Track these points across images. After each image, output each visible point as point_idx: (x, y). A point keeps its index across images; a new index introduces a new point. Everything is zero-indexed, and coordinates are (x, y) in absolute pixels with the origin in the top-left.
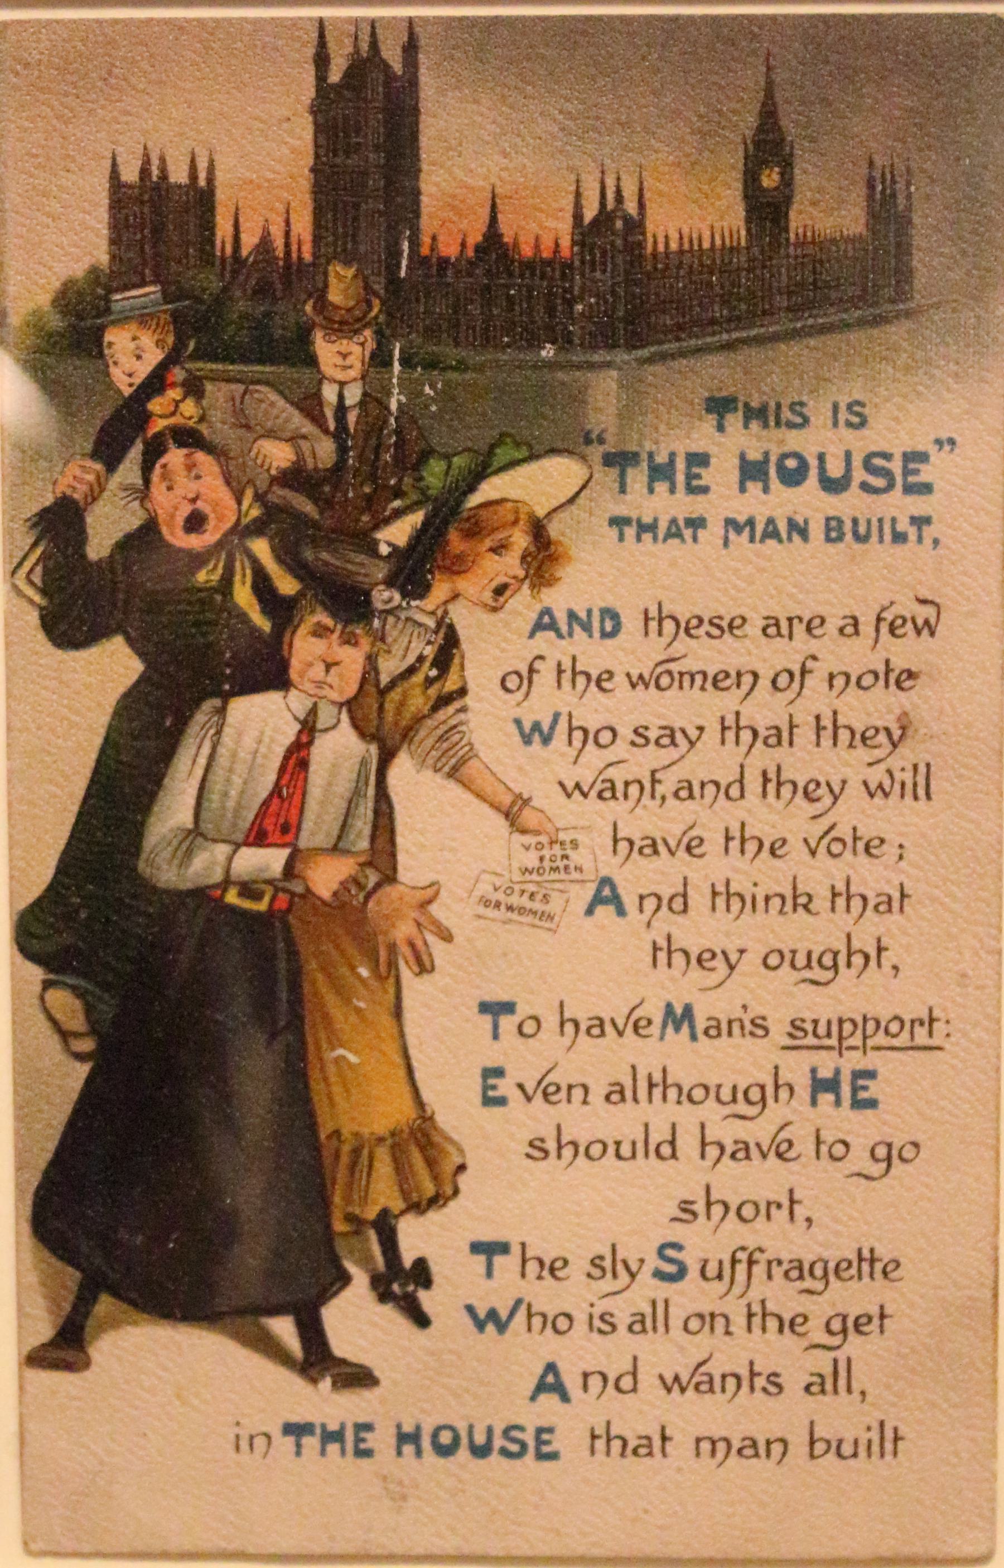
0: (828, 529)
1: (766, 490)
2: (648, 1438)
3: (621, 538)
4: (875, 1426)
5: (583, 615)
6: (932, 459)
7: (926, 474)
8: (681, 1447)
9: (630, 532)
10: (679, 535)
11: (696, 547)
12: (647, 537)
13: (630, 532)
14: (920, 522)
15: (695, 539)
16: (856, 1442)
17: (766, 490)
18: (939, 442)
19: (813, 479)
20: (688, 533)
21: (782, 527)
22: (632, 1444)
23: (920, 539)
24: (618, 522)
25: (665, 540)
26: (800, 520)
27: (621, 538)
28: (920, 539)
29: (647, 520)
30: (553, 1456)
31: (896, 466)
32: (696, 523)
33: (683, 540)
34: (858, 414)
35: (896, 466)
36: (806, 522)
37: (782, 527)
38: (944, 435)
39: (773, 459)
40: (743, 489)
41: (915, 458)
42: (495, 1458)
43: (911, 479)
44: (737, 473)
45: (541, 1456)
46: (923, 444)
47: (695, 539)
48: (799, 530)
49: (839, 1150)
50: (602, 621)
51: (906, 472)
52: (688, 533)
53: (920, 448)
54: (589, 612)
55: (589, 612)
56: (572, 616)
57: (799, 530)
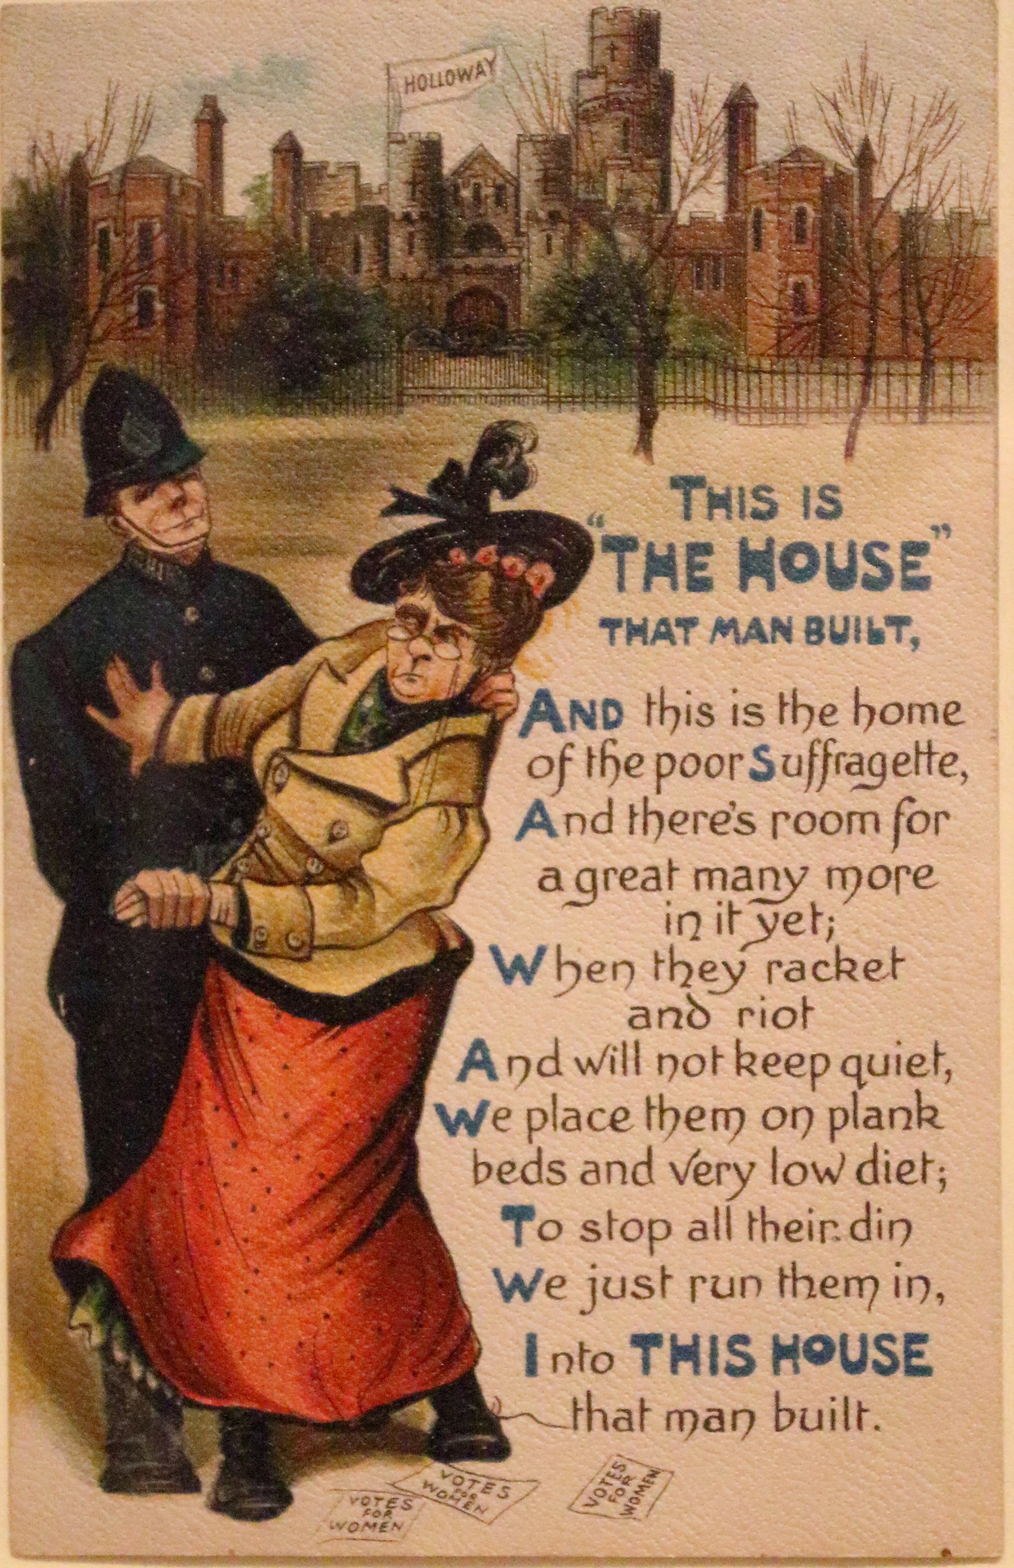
0: (808, 633)
1: (771, 586)
2: (628, 1412)
3: (612, 638)
4: (840, 1400)
5: (586, 706)
6: (933, 547)
7: (927, 564)
8: (655, 1418)
9: (621, 633)
10: (668, 636)
11: (688, 648)
12: (637, 641)
13: (621, 633)
14: (899, 622)
15: (686, 641)
16: (820, 1413)
17: (771, 586)
18: (935, 528)
19: (822, 575)
20: (678, 632)
21: (767, 628)
22: (612, 1416)
23: (899, 639)
24: (610, 624)
25: (654, 640)
26: (784, 620)
27: (612, 638)
28: (899, 639)
29: (637, 621)
30: (926, 1371)
31: (893, 559)
32: (688, 623)
33: (673, 643)
34: (832, 501)
35: (893, 559)
36: (790, 619)
37: (767, 628)
38: (939, 523)
39: (778, 550)
40: (744, 586)
41: (915, 548)
42: (869, 1372)
43: (911, 573)
44: (736, 569)
45: (913, 1371)
46: (921, 534)
47: (686, 641)
48: (783, 629)
49: (550, 1230)
50: (605, 713)
51: (906, 566)
52: (678, 632)
53: (918, 538)
54: (593, 704)
55: (593, 704)
56: (575, 707)
57: (783, 629)
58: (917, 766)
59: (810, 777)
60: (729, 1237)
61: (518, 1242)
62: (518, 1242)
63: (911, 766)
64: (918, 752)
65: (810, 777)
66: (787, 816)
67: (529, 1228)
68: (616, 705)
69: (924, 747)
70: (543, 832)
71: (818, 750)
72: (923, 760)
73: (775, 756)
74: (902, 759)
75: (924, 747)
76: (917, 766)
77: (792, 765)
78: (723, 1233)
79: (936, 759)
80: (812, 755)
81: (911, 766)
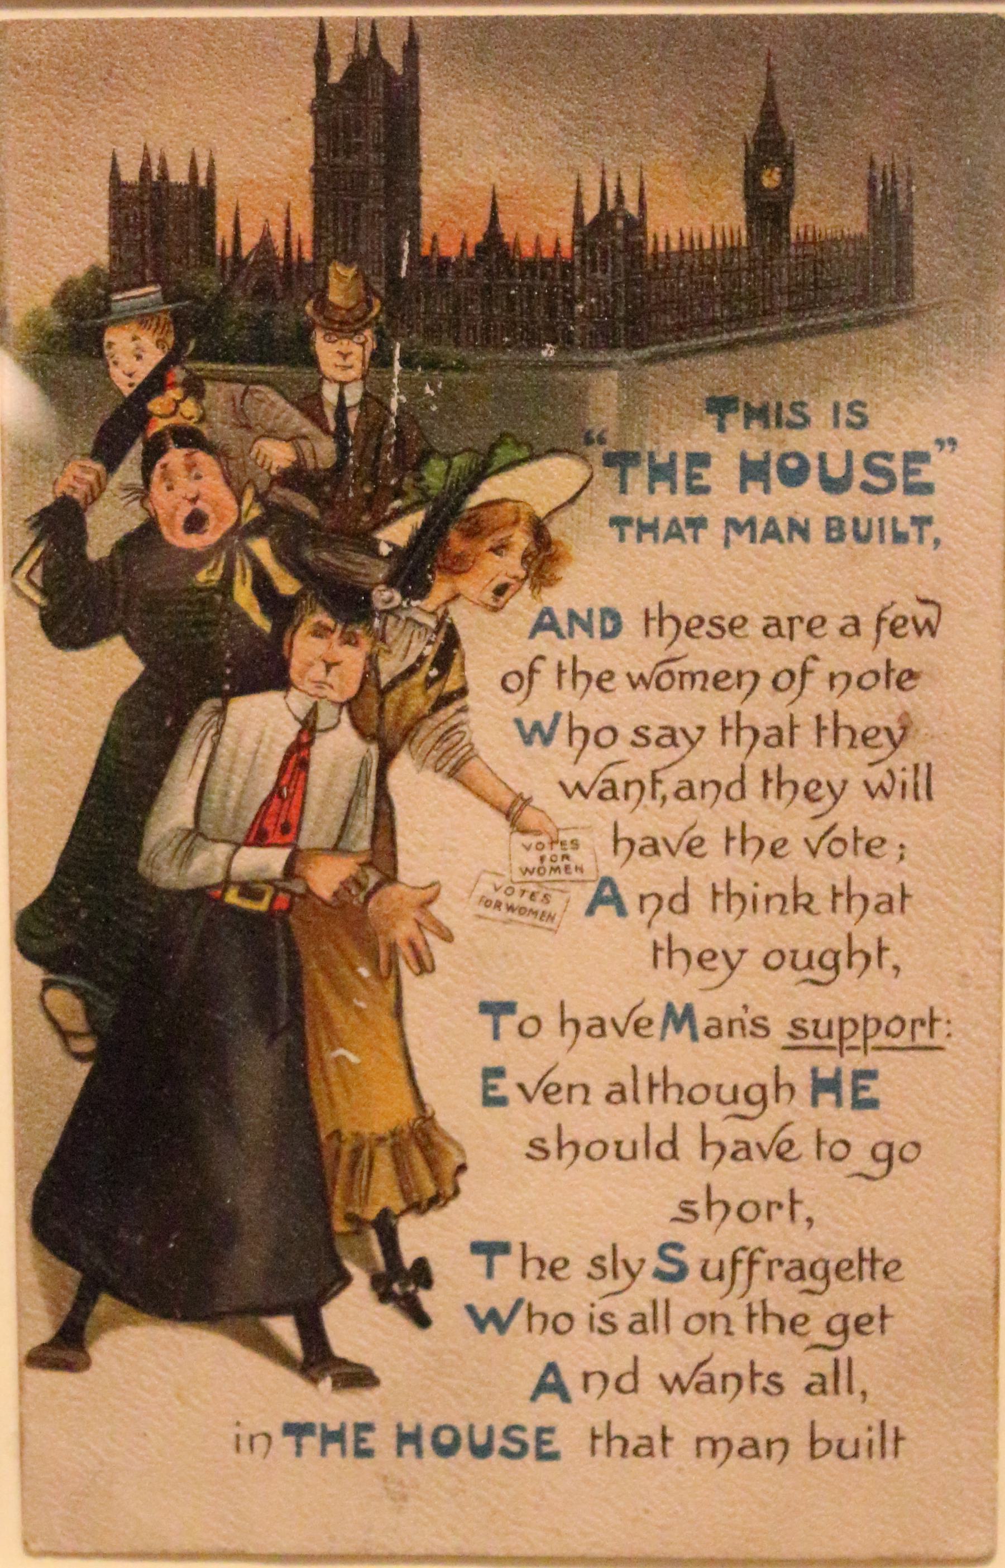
0: (829, 529)
5: (583, 615)
9: (631, 532)
10: (679, 535)
11: (697, 547)
12: (648, 537)
13: (631, 532)
14: (921, 522)
15: (696, 539)
20: (688, 533)
21: (783, 527)
23: (921, 539)
24: (619, 522)
25: (666, 540)
26: (801, 520)
28: (921, 539)
29: (648, 520)
32: (697, 523)
33: (684, 540)
34: (859, 414)
36: (807, 522)
37: (783, 527)
47: (696, 539)
48: (800, 530)
50: (603, 621)
52: (688, 533)
54: (590, 612)
55: (590, 612)
56: (572, 616)
57: (800, 530)
58: (860, 1270)
59: (733, 1282)
60: (668, 1330)
61: (496, 1036)
62: (496, 1036)
63: (854, 1271)
64: (861, 1259)
65: (733, 1282)
66: (801, 619)
67: (508, 1023)
68: (616, 616)
69: (867, 1254)
70: (552, 634)
71: (743, 1256)
72: (866, 1267)
73: (691, 1258)
74: (845, 1265)
75: (867, 1254)
76: (860, 1270)
77: (712, 1270)
78: (662, 1328)
79: (879, 1267)
80: (735, 1261)
81: (854, 1271)
